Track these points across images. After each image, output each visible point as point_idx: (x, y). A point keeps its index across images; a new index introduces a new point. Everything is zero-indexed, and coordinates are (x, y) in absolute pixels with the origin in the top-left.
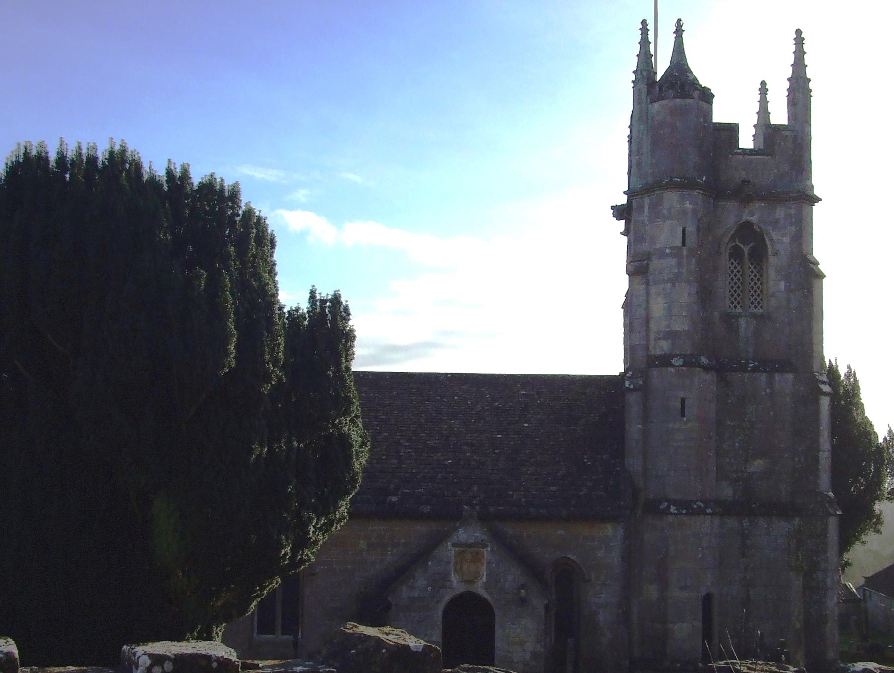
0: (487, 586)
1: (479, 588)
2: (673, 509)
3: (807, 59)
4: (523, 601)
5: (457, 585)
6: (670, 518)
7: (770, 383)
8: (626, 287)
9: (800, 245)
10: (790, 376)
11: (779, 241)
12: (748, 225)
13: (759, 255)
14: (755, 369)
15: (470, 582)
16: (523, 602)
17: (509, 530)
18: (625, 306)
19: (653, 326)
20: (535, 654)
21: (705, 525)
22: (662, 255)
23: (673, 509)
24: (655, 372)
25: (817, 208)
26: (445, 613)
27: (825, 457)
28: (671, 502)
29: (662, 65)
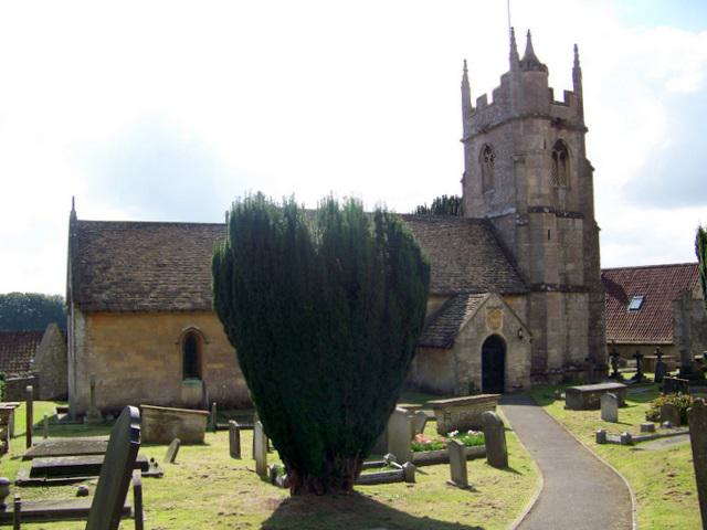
0: (504, 330)
1: (499, 332)
2: (549, 288)
3: (580, 59)
4: (521, 337)
5: (490, 332)
6: (548, 294)
7: (574, 222)
8: (463, 170)
9: (584, 154)
10: (581, 221)
11: (573, 150)
12: (560, 141)
13: (564, 156)
14: (568, 216)
15: (495, 328)
16: (521, 337)
17: (509, 301)
18: (463, 181)
19: (530, 191)
20: (527, 367)
21: (533, 304)
22: (534, 152)
23: (549, 288)
24: (533, 215)
25: (461, 137)
26: (484, 346)
27: (65, 439)
28: (547, 285)
29: (522, 53)
